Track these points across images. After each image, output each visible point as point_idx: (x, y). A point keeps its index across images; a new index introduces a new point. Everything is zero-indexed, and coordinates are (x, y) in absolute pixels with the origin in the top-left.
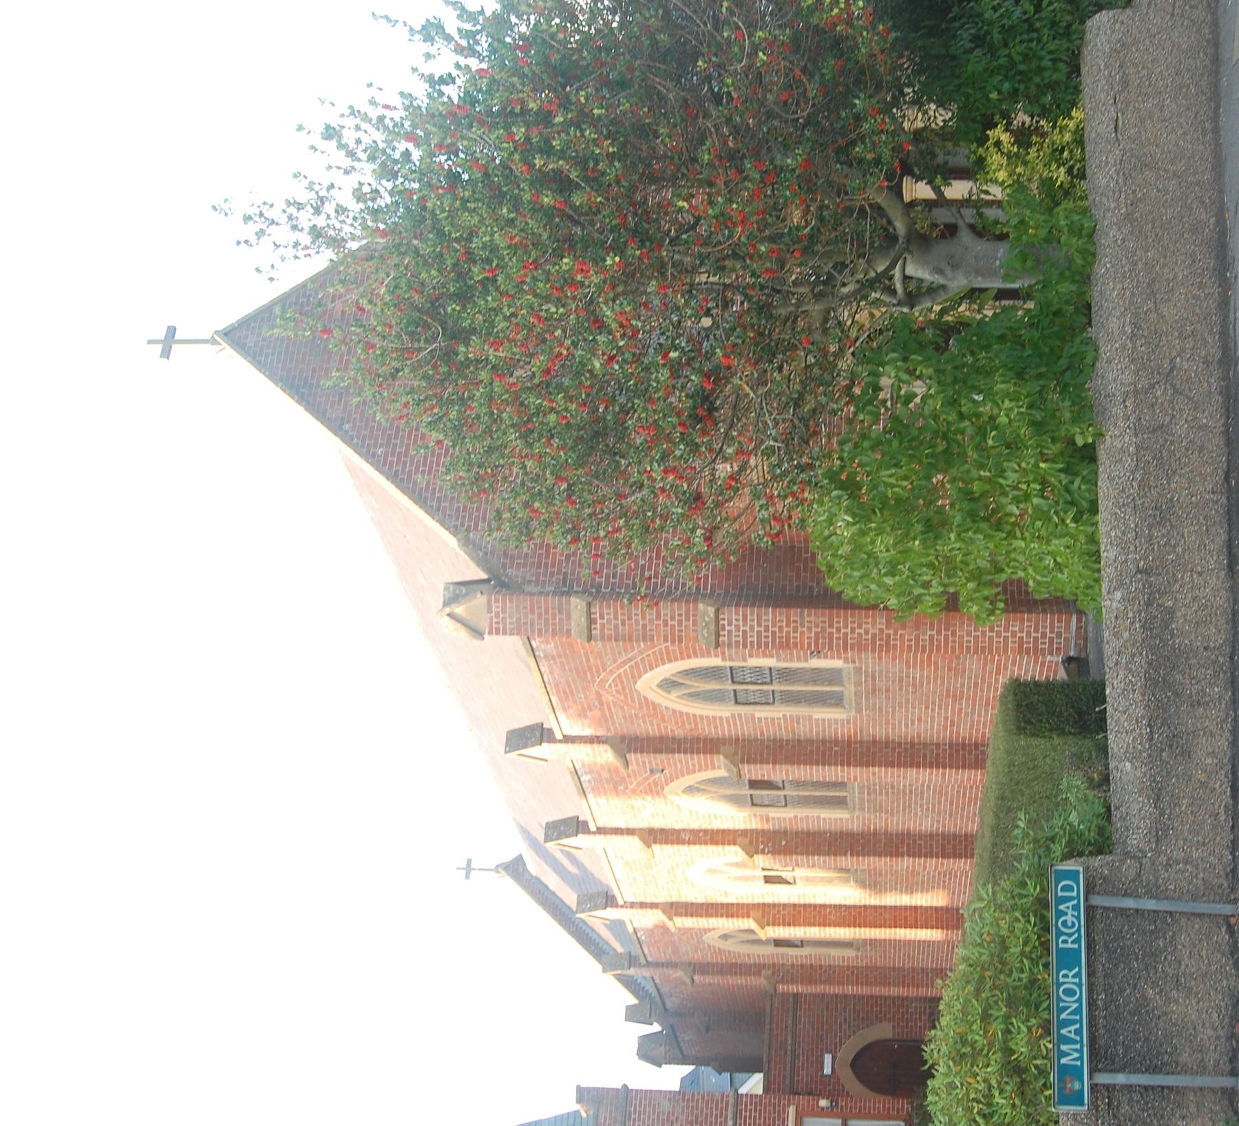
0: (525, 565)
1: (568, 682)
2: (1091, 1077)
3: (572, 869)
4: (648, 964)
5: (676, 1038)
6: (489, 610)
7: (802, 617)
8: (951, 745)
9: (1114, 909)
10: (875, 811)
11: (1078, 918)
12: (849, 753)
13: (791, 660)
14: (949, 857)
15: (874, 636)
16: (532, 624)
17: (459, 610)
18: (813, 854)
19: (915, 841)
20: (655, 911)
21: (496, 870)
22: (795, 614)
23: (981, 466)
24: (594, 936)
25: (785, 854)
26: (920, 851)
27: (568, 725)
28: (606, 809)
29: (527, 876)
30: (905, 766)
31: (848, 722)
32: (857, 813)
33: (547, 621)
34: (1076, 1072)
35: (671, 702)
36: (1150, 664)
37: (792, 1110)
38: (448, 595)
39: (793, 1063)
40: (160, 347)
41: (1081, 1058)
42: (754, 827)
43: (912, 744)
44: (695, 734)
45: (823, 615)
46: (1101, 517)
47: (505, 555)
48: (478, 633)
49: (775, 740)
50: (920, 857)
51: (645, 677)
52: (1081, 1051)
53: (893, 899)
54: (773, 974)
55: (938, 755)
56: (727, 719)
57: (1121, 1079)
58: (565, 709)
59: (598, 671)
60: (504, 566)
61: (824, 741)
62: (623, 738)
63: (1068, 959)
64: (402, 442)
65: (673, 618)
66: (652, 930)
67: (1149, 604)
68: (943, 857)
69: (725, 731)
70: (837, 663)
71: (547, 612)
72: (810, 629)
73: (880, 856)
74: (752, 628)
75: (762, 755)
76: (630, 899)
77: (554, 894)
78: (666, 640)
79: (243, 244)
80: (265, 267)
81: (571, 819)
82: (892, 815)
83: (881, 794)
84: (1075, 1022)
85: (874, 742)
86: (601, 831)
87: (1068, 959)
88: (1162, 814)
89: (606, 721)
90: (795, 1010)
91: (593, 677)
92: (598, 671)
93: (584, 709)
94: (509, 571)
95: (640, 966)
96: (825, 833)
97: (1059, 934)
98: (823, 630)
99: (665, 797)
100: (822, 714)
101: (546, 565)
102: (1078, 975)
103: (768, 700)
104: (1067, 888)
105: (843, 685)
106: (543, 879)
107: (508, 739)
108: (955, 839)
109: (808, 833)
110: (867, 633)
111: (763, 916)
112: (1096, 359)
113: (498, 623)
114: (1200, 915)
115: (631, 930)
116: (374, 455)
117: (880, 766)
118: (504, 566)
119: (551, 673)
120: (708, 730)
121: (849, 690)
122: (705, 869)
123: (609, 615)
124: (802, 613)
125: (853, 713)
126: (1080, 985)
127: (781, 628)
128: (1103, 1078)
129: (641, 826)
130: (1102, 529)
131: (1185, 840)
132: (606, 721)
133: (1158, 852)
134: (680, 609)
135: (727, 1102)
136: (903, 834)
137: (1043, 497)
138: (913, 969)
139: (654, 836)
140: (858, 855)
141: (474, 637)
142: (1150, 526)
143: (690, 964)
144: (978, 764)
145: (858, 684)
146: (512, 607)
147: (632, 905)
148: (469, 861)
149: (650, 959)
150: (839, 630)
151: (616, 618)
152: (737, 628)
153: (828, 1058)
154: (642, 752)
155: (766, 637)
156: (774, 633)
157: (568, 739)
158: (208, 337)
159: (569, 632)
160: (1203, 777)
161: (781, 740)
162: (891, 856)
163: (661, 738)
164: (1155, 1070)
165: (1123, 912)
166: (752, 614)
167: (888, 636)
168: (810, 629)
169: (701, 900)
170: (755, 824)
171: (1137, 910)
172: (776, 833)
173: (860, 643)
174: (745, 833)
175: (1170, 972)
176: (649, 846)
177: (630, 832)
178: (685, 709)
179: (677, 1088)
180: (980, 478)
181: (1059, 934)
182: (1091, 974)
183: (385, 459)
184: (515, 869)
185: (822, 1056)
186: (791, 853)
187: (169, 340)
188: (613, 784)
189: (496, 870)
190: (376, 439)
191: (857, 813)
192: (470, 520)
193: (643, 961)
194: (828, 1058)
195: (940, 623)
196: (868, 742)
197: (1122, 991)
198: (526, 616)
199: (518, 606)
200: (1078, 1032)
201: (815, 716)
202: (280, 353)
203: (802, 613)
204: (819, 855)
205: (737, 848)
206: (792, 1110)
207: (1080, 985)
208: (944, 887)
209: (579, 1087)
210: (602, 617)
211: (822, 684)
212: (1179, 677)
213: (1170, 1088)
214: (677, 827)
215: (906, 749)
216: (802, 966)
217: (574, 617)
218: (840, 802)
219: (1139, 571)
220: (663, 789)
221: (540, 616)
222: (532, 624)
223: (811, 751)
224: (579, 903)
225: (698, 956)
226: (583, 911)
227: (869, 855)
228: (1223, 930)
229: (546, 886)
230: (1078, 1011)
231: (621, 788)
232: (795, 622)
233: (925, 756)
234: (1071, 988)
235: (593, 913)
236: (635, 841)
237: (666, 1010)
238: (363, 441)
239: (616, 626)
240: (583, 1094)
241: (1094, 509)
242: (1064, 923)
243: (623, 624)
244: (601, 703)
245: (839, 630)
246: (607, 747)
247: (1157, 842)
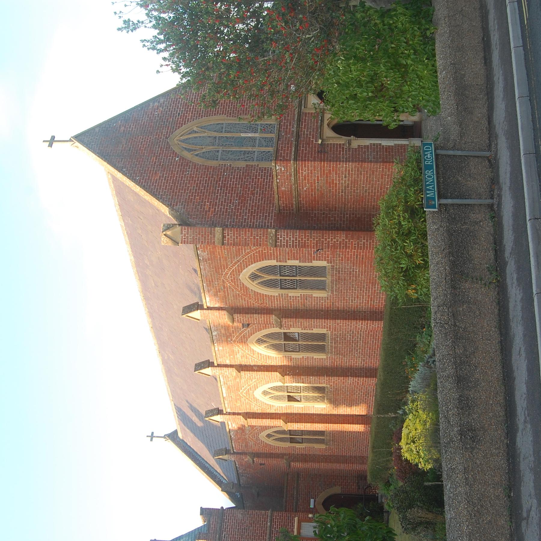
0: (196, 218)
2: (438, 200)
3: (200, 424)
4: (234, 453)
6: (182, 233)
7: (311, 234)
9: (445, 155)
10: (337, 354)
11: (432, 156)
12: (327, 314)
13: (306, 262)
14: (368, 377)
15: (340, 242)
16: (199, 239)
17: (169, 233)
19: (354, 371)
20: (239, 416)
22: (308, 233)
24: (207, 465)
25: (298, 375)
26: (356, 375)
27: (208, 301)
28: (221, 353)
36: (456, 89)
37: (296, 519)
38: (165, 228)
39: (297, 503)
40: (48, 143)
41: (435, 195)
42: (285, 364)
43: (354, 311)
44: (263, 306)
45: (320, 233)
48: (176, 243)
49: (296, 310)
50: (356, 377)
51: (244, 271)
52: (434, 193)
53: (344, 410)
54: (289, 457)
55: (365, 315)
56: (277, 296)
57: (450, 201)
58: (209, 292)
59: (224, 269)
60: (188, 218)
62: (232, 308)
63: (429, 167)
64: (147, 175)
65: (257, 236)
69: (276, 304)
70: (323, 263)
71: (205, 234)
72: (314, 239)
73: (339, 376)
74: (290, 238)
75: (291, 315)
77: (190, 447)
78: (254, 245)
79: (114, 2)
81: (206, 361)
82: (344, 357)
83: (340, 344)
84: (432, 185)
85: (338, 310)
86: (219, 366)
87: (429, 167)
88: (463, 129)
90: (298, 480)
91: (222, 272)
92: (224, 269)
94: (190, 220)
95: (231, 454)
96: (315, 367)
97: (425, 160)
99: (248, 345)
100: (317, 294)
101: (205, 218)
103: (294, 285)
105: (326, 277)
106: (185, 440)
107: (183, 310)
108: (371, 370)
109: (308, 367)
110: (337, 241)
111: (287, 419)
112: (434, 11)
113: (185, 239)
114: (478, 157)
115: (228, 430)
116: (135, 179)
117: (341, 319)
119: (205, 269)
120: (268, 304)
121: (328, 279)
124: (311, 232)
125: (330, 294)
126: (433, 175)
127: (302, 239)
128: (443, 201)
130: (438, 64)
131: (471, 137)
134: (260, 232)
135: (267, 515)
136: (349, 368)
137: (415, 55)
138: (351, 456)
139: (241, 368)
140: (329, 376)
141: (175, 245)
143: (252, 453)
146: (190, 232)
148: (153, 433)
149: (235, 451)
150: (326, 239)
153: (312, 501)
154: (240, 314)
155: (296, 243)
158: (68, 139)
159: (214, 242)
161: (299, 309)
162: (344, 376)
163: (248, 308)
165: (449, 156)
168: (314, 239)
169: (259, 411)
170: (285, 363)
172: (294, 367)
173: (334, 245)
174: (281, 367)
175: (467, 173)
176: (239, 372)
177: (231, 366)
178: (259, 291)
180: (392, 48)
181: (425, 160)
182: (438, 173)
183: (140, 181)
184: (173, 436)
185: (310, 501)
187: (152, 436)
188: (226, 336)
190: (136, 174)
192: (174, 202)
194: (312, 501)
195: (367, 237)
197: (449, 178)
199: (193, 231)
202: (97, 144)
203: (311, 232)
204: (313, 376)
205: (278, 374)
206: (296, 519)
207: (433, 175)
209: (201, 508)
210: (228, 235)
213: (468, 205)
215: (351, 313)
216: (302, 454)
217: (216, 236)
218: (321, 349)
219: (451, 64)
220: (247, 340)
221: (202, 235)
222: (199, 239)
223: (312, 314)
224: (206, 413)
227: (334, 376)
228: (487, 161)
229: (187, 444)
231: (229, 339)
232: (308, 236)
233: (359, 316)
235: (211, 418)
237: (240, 485)
238: (131, 174)
239: (234, 239)
241: (434, 56)
242: (427, 158)
243: (237, 238)
244: (224, 288)
245: (326, 239)
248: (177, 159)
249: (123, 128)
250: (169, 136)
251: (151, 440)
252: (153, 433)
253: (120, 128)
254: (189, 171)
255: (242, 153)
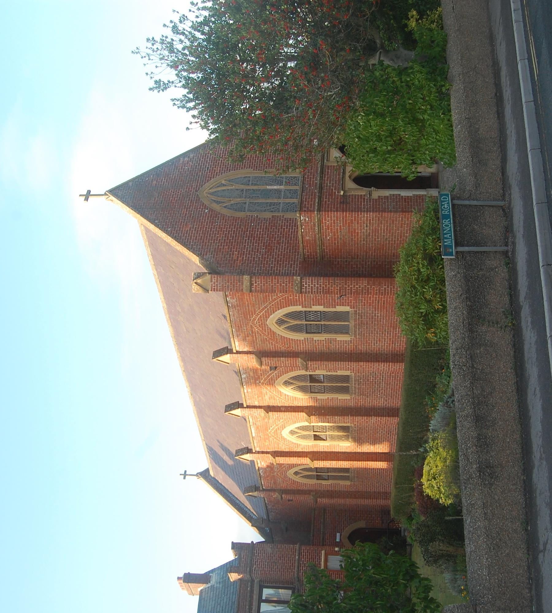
1: (240, 320)
5: (273, 538)
6: (211, 281)
8: (392, 354)
9: (462, 205)
11: (449, 206)
13: (330, 308)
14: (391, 416)
15: (362, 288)
17: (199, 281)
18: (335, 416)
21: (197, 475)
22: (331, 280)
23: (410, 99)
27: (237, 345)
28: (250, 394)
29: (210, 477)
30: (374, 362)
31: (351, 341)
32: (353, 396)
33: (234, 285)
36: (471, 142)
37: (323, 552)
38: (195, 276)
41: (452, 243)
43: (377, 354)
44: (289, 349)
45: (343, 280)
46: (452, 113)
47: (218, 263)
50: (379, 416)
51: (271, 317)
52: (452, 241)
58: (238, 337)
59: (252, 315)
60: (217, 267)
61: (341, 353)
62: (260, 352)
63: (446, 217)
65: (283, 283)
66: (265, 469)
67: (470, 126)
68: (388, 416)
69: (302, 348)
70: (347, 309)
71: (234, 282)
72: (337, 286)
73: (362, 416)
76: (258, 449)
80: (149, 73)
81: (236, 403)
82: (368, 397)
86: (248, 407)
87: (446, 217)
88: (478, 180)
89: (254, 342)
91: (250, 317)
93: (245, 337)
94: (219, 269)
97: (442, 210)
98: (343, 286)
100: (341, 338)
101: (234, 267)
103: (319, 330)
112: (449, 69)
114: (493, 206)
115: (257, 468)
116: (167, 231)
118: (217, 267)
119: (234, 315)
121: (351, 324)
122: (290, 431)
123: (258, 282)
125: (353, 337)
127: (326, 285)
128: (460, 249)
129: (265, 405)
130: (453, 119)
132: (254, 342)
134: (286, 279)
139: (269, 409)
142: (470, 107)
143: (281, 490)
144: (402, 361)
145: (355, 320)
147: (259, 452)
148: (185, 471)
150: (349, 286)
151: (261, 283)
152: (309, 285)
153: (338, 535)
154: (268, 357)
155: (320, 289)
156: (323, 287)
157: (238, 352)
158: (103, 193)
160: (492, 171)
162: (367, 416)
166: (315, 280)
167: (368, 288)
168: (337, 286)
169: (287, 450)
170: (311, 404)
171: (470, 205)
173: (357, 291)
174: (307, 407)
181: (442, 210)
184: (205, 475)
186: (326, 415)
187: (185, 475)
188: (255, 378)
189: (197, 475)
191: (353, 396)
192: (204, 252)
193: (261, 489)
194: (338, 535)
195: (388, 283)
196: (359, 353)
197: (465, 227)
198: (226, 284)
199: (223, 279)
201: (338, 339)
203: (334, 279)
204: (337, 416)
205: (304, 414)
206: (323, 552)
207: (450, 224)
208: (388, 440)
209: (232, 542)
210: (256, 283)
211: (341, 321)
212: (481, 145)
213: (484, 252)
214: (279, 405)
216: (328, 491)
217: (244, 284)
219: (466, 118)
220: (275, 382)
225: (284, 486)
226: (238, 456)
231: (258, 382)
232: (332, 283)
233: (381, 358)
234: (448, 225)
235: (241, 457)
236: (262, 412)
240: (236, 546)
242: (444, 208)
243: (264, 285)
244: (252, 333)
245: (349, 286)
246: (254, 356)
248: (206, 211)
249: (155, 182)
250: (199, 189)
251: (184, 478)
252: (185, 471)
253: (152, 182)
254: (217, 222)
255: (268, 204)
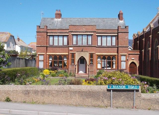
11: (132, 88)
34: (112, 87)
35: (155, 41)
52: (115, 88)
102: (125, 88)
104: (136, 87)
126: (123, 88)
133: (142, 99)
164: (113, 98)
179: (4, 48)
200: (117, 88)
207: (123, 88)
230: (120, 88)
242: (131, 86)
247: (143, 99)
